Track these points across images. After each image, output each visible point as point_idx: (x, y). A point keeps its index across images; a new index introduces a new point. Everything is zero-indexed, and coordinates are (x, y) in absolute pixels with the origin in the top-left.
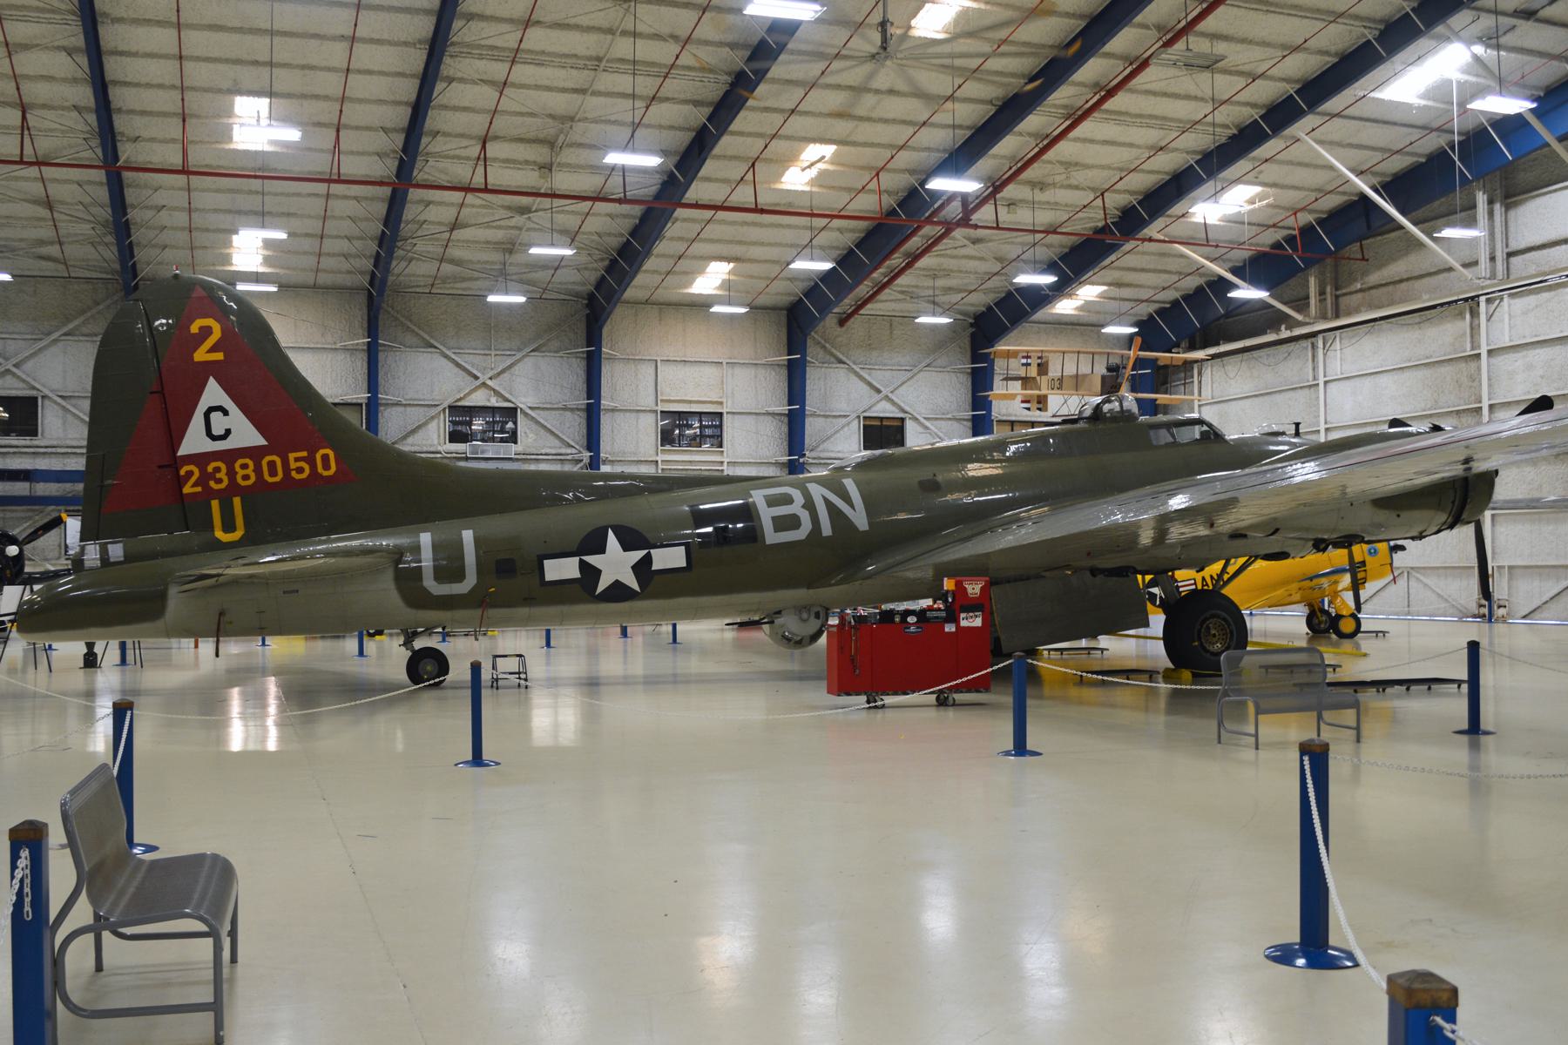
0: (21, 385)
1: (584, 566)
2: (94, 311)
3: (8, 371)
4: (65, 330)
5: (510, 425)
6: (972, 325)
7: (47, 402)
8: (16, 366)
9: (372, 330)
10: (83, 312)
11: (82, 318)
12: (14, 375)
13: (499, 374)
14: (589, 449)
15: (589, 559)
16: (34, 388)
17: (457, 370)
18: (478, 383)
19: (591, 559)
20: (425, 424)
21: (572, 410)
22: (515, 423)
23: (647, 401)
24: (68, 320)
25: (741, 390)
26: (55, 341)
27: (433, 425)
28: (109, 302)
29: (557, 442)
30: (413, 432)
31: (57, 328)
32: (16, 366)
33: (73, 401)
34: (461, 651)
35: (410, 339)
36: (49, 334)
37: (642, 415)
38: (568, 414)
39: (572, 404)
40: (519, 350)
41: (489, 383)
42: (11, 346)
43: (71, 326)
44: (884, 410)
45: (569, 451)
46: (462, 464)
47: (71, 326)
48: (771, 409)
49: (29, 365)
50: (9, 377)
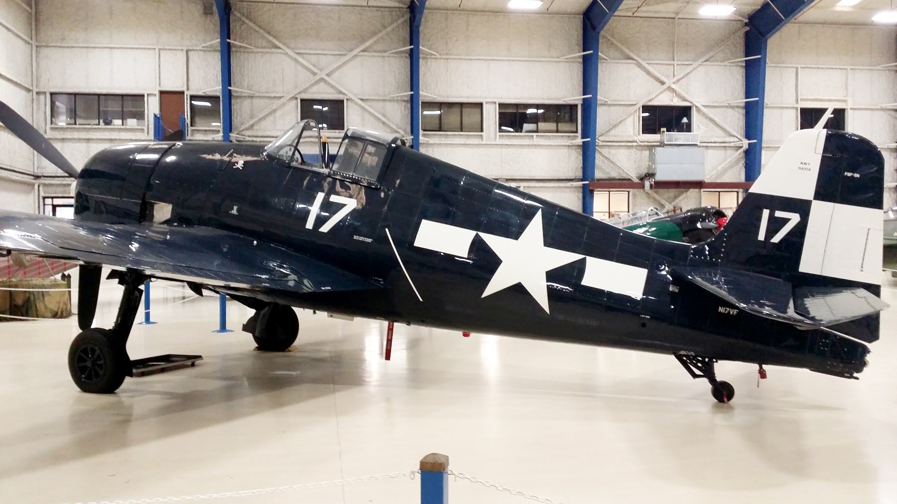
0: (332, 90)
1: (478, 246)
2: (384, 32)
3: (322, 79)
4: (363, 47)
5: (685, 120)
6: (746, 24)
7: (350, 103)
8: (328, 75)
9: (226, 31)
10: (375, 34)
11: (375, 39)
12: (326, 82)
13: (678, 80)
14: (748, 137)
15: (490, 240)
16: (341, 92)
17: (648, 77)
18: (665, 86)
19: (494, 242)
20: (625, 119)
21: (733, 107)
22: (689, 119)
23: (790, 100)
24: (363, 40)
25: (710, 88)
26: (356, 56)
27: (630, 121)
28: (395, 25)
29: (722, 133)
30: (615, 126)
31: (357, 46)
32: (328, 75)
33: (369, 103)
34: (313, 324)
35: (261, 42)
36: (351, 50)
37: (785, 111)
38: (730, 110)
39: (734, 102)
40: (694, 60)
41: (674, 86)
42: (323, 61)
43: (367, 44)
44: (665, 100)
45: (732, 139)
46: (139, 157)
47: (367, 44)
48: (885, 105)
49: (336, 75)
50: (322, 84)
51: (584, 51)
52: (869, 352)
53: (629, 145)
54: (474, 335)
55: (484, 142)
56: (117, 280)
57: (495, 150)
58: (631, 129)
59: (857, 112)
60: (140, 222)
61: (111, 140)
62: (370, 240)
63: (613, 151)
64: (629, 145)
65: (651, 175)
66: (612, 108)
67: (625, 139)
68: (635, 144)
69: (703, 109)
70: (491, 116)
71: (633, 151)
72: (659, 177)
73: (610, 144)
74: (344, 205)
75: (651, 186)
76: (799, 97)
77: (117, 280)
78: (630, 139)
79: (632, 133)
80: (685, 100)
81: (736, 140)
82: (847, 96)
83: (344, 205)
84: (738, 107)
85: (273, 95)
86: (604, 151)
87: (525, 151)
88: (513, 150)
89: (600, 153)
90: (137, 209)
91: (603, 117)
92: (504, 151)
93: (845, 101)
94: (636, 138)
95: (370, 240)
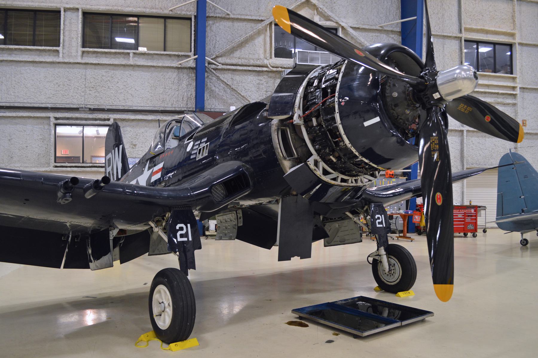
37: (447, 41)
51: (402, 19)
52: (200, 248)
53: (258, 70)
55: (60, 60)
56: (196, 252)
57: (78, 72)
58: (261, 52)
59: (525, 48)
61: (488, 86)
63: (238, 77)
64: (258, 70)
66: (237, 24)
67: (252, 62)
68: (265, 69)
69: (351, 31)
70: (72, 29)
73: (234, 69)
76: (463, 26)
77: (196, 252)
78: (258, 63)
79: (262, 56)
80: (328, 18)
82: (514, 29)
83: (148, 170)
84: (392, 32)
86: (226, 77)
87: (119, 73)
88: (102, 72)
89: (218, 78)
91: (219, 36)
92: (90, 72)
93: (512, 35)
94: (266, 62)
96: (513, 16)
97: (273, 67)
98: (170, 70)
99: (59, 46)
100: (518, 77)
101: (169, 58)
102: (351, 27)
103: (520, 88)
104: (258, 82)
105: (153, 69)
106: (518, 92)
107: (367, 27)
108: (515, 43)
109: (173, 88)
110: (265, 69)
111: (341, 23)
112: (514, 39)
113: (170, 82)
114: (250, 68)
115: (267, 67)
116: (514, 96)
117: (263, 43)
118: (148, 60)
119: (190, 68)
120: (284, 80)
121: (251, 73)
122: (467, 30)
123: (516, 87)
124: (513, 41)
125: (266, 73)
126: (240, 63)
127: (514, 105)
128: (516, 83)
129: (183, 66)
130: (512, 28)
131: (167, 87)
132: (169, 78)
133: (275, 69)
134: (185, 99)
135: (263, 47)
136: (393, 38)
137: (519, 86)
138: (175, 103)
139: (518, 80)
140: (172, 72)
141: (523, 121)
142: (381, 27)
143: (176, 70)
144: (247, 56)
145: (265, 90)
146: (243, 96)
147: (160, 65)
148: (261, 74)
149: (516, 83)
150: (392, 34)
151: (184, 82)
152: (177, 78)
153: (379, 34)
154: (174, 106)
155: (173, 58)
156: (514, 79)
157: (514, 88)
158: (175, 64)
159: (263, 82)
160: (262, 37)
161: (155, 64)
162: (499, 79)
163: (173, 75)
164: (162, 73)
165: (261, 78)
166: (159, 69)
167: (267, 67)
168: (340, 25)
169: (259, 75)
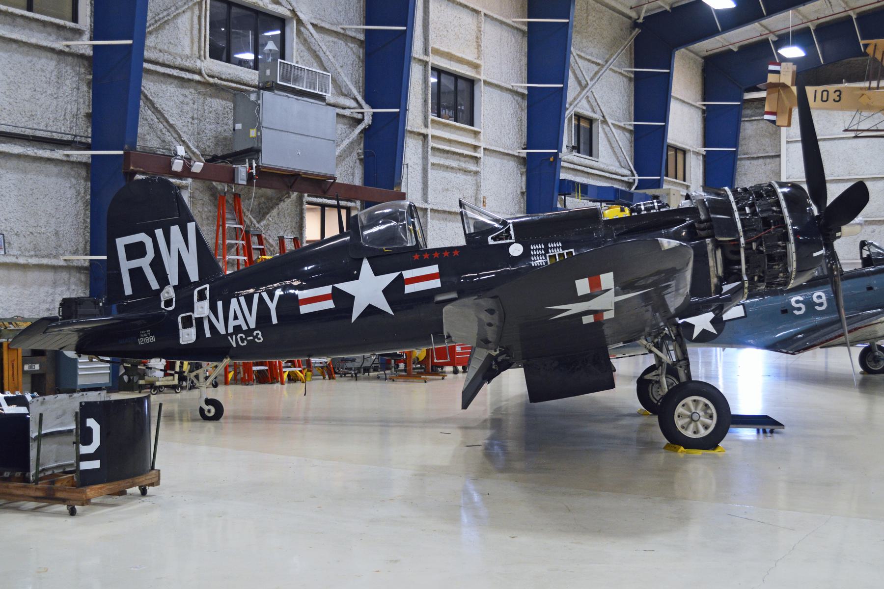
14: (370, 100)
51: (528, 83)
54: (727, 349)
58: (186, 42)
60: (497, 410)
61: (450, 141)
62: (815, 254)
63: (613, 168)
65: (254, 152)
67: (179, 62)
68: (197, 77)
71: (190, 93)
72: (268, 159)
74: (272, 301)
75: (250, 177)
78: (188, 64)
79: (187, 51)
81: (353, 104)
83: (272, 301)
85: (755, 156)
90: (139, 492)
93: (476, 67)
94: (199, 64)
95: (815, 254)
96: (477, 38)
97: (209, 76)
98: (44, 54)
99: (809, 28)
100: (482, 131)
101: (42, 28)
102: (312, 24)
103: (485, 149)
104: (181, 98)
105: (14, 46)
106: (480, 154)
107: (327, 26)
108: (689, 151)
109: (49, 92)
110: (197, 77)
111: (299, 14)
112: (478, 73)
113: (44, 79)
114: (175, 72)
115: (200, 73)
116: (476, 159)
117: (189, 27)
118: (5, 24)
119: (82, 56)
120: (757, 81)
121: (171, 80)
122: (437, 52)
123: (480, 147)
124: (478, 77)
125: (194, 84)
126: (161, 60)
127: (476, 173)
128: (479, 140)
129: (72, 51)
130: (476, 56)
131: (38, 89)
132: (43, 71)
133: (211, 80)
134: (68, 117)
135: (189, 34)
136: (351, 49)
137: (483, 145)
138: (51, 123)
139: (481, 136)
140: (47, 58)
141: (484, 198)
142: (343, 29)
143: (55, 56)
144: (166, 48)
145: (191, 114)
146: (171, 126)
147: (33, 41)
148: (186, 84)
149: (479, 140)
150: (352, 42)
151: (68, 82)
152: (55, 73)
153: (336, 40)
154: (49, 129)
155: (49, 29)
156: (476, 134)
157: (475, 148)
158: (60, 45)
159: (188, 100)
160: (188, 15)
161: (24, 38)
162: (461, 132)
163: (49, 64)
164: (29, 58)
165: (186, 92)
166: (26, 49)
167: (200, 73)
168: (296, 15)
169: (182, 87)
